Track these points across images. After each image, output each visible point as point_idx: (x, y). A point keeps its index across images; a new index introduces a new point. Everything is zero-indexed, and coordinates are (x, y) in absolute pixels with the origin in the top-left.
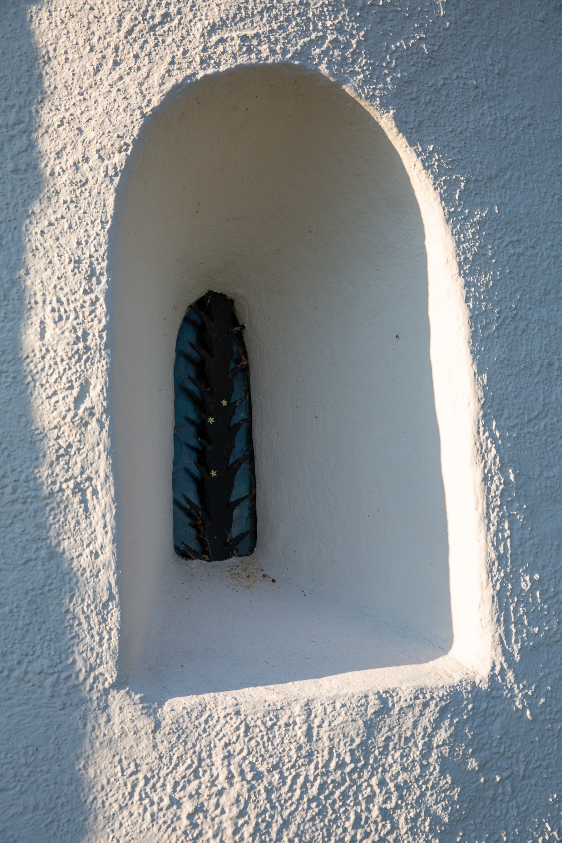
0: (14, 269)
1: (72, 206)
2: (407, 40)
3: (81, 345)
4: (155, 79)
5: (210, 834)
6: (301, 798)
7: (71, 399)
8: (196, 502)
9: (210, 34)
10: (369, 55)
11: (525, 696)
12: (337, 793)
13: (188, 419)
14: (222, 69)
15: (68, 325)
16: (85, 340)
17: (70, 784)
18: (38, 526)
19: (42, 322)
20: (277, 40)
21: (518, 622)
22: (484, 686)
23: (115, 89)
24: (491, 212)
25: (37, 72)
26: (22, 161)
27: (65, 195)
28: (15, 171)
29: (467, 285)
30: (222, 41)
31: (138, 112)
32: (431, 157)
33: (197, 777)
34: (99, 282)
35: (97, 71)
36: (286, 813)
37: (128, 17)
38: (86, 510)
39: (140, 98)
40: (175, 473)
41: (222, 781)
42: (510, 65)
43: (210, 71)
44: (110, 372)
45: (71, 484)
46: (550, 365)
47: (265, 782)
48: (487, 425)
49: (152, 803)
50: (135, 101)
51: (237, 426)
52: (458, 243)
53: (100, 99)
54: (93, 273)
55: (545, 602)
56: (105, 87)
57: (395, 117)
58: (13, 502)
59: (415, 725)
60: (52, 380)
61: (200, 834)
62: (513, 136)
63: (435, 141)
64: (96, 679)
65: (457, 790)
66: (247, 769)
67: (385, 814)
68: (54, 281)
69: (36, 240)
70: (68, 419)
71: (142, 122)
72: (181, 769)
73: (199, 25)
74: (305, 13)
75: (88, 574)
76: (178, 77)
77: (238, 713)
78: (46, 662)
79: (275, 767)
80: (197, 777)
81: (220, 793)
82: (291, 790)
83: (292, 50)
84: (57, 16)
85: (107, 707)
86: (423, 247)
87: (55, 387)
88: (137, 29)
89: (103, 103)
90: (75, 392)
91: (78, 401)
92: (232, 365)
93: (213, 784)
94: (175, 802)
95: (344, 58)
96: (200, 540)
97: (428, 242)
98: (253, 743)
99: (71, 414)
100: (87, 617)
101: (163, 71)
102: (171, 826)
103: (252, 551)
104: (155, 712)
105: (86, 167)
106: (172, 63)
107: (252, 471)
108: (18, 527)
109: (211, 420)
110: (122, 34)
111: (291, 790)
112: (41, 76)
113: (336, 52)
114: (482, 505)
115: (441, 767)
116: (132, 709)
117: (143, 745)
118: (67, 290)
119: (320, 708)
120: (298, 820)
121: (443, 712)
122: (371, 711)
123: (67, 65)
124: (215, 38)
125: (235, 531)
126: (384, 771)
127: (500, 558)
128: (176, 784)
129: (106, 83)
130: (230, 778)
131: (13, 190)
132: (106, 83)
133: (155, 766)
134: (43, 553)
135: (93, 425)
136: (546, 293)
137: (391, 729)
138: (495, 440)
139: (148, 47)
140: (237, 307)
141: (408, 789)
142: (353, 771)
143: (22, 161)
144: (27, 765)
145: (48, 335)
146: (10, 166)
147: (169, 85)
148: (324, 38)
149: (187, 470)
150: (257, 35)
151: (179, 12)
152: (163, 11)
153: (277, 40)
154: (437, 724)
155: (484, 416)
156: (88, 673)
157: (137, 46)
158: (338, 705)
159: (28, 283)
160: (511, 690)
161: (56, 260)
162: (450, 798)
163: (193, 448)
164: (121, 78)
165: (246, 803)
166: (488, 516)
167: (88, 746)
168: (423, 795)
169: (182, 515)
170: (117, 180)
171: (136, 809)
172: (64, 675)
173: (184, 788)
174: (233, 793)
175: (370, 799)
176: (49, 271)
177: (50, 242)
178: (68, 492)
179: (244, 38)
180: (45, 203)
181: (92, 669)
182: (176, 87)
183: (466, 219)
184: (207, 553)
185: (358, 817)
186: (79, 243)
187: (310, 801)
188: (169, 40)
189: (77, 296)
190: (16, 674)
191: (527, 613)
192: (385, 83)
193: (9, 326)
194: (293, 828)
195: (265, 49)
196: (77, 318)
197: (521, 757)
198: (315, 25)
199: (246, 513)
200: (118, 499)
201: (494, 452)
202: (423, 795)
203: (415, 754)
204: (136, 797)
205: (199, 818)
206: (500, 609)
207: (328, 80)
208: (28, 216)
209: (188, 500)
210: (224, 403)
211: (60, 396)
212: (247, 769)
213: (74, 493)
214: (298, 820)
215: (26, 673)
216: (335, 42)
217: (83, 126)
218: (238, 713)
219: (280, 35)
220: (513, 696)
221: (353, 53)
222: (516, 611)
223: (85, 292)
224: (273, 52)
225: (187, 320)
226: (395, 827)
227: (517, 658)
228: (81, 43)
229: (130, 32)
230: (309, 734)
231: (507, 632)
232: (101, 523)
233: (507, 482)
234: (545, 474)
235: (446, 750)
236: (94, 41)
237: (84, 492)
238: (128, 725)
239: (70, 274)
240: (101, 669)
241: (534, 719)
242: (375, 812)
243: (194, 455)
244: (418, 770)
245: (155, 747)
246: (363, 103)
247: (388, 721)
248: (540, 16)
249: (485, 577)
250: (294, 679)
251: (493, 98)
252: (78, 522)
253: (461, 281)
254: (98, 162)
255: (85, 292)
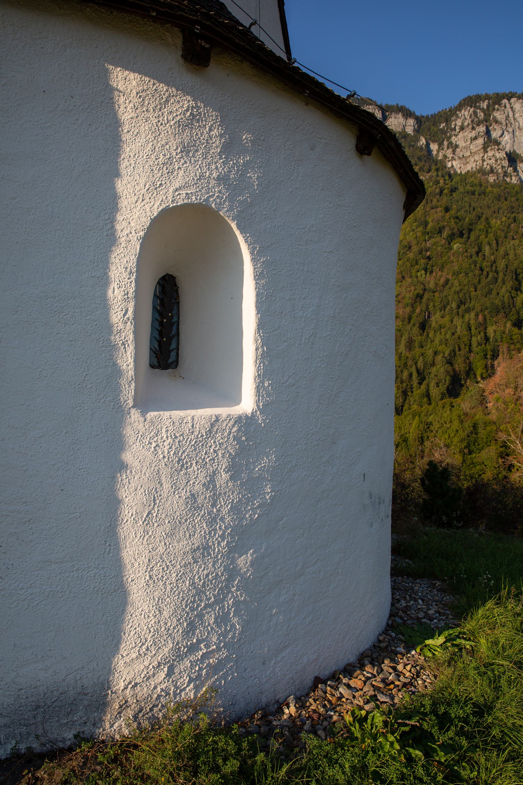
0: (105, 269)
1: (125, 249)
2: (243, 197)
3: (126, 297)
4: (156, 206)
5: (160, 453)
6: (189, 445)
7: (122, 314)
8: (157, 348)
9: (175, 192)
10: (229, 202)
11: (262, 419)
12: (200, 444)
13: (157, 319)
14: (179, 204)
15: (122, 289)
16: (128, 295)
17: (118, 435)
18: (110, 355)
19: (114, 288)
20: (198, 195)
21: (263, 396)
22: (250, 415)
23: (142, 209)
24: (267, 259)
25: (116, 202)
26: (110, 232)
27: (123, 245)
28: (107, 236)
29: (256, 283)
30: (179, 194)
31: (149, 218)
32: (248, 238)
33: (157, 436)
34: (133, 275)
35: (136, 202)
36: (184, 449)
37: (148, 184)
38: (125, 351)
39: (150, 213)
40: (151, 338)
41: (165, 438)
42: (278, 207)
43: (174, 205)
44: (135, 306)
45: (121, 342)
46: (282, 312)
47: (178, 439)
48: (259, 332)
49: (143, 443)
50: (149, 214)
51: (174, 323)
52: (255, 269)
53: (137, 212)
54: (131, 272)
55: (272, 390)
56: (138, 208)
57: (237, 224)
58: (102, 347)
59: (226, 426)
60: (116, 307)
61: (157, 453)
62: (277, 232)
63: (250, 233)
64: (127, 404)
65: (238, 446)
66: (173, 435)
67: (215, 451)
68: (118, 274)
69: (113, 260)
70: (121, 321)
71: (150, 221)
72: (152, 433)
73: (172, 188)
74: (208, 186)
75: (125, 371)
76: (164, 206)
77: (171, 418)
78: (111, 398)
79: (182, 435)
80: (157, 436)
81: (164, 441)
82: (186, 442)
83: (203, 198)
84: (124, 182)
85: (130, 413)
86: (243, 268)
87: (117, 310)
88: (151, 189)
89: (138, 214)
90: (124, 312)
91: (125, 315)
92: (174, 301)
93: (162, 439)
94: (150, 443)
95: (221, 202)
96: (158, 362)
97: (245, 267)
98: (175, 427)
99: (122, 319)
100: (125, 385)
101: (159, 204)
102: (148, 450)
103: (176, 367)
104: (145, 416)
105: (131, 235)
106: (162, 201)
107: (178, 339)
108: (103, 355)
109: (165, 320)
110: (145, 190)
111: (186, 442)
112: (117, 203)
113: (218, 200)
114: (255, 358)
115: (234, 438)
116: (138, 414)
117: (141, 425)
118: (122, 277)
119: (197, 419)
120: (188, 451)
121: (236, 422)
122: (213, 420)
123: (126, 200)
124: (177, 193)
125: (170, 361)
126: (216, 439)
127: (259, 375)
128: (151, 438)
129: (139, 207)
130: (167, 437)
131: (106, 242)
132: (139, 207)
133: (144, 432)
134: (111, 364)
135: (129, 323)
136: (283, 288)
137: (219, 426)
138: (261, 337)
139: (154, 195)
140: (176, 280)
141: (223, 444)
142: (206, 438)
143: (110, 232)
144: (105, 428)
145: (115, 292)
146: (105, 234)
147: (160, 209)
148: (214, 195)
149: (155, 337)
150: (191, 193)
151: (165, 183)
152: (160, 183)
153: (198, 195)
154: (233, 426)
155: (258, 328)
156: (124, 402)
157: (150, 195)
158: (203, 418)
159: (110, 274)
160: (258, 417)
161: (119, 267)
162: (236, 448)
163: (158, 330)
164: (144, 205)
165: (172, 445)
166: (256, 361)
167: (124, 424)
168: (227, 446)
169: (152, 353)
170: (141, 241)
171: (138, 444)
172: (117, 402)
173: (153, 439)
174: (168, 442)
175: (210, 447)
176: (117, 271)
177: (118, 261)
178: (120, 345)
179: (187, 194)
180: (116, 247)
181: (126, 401)
182: (163, 210)
183: (258, 260)
184: (161, 367)
185: (206, 452)
186: (127, 262)
187: (192, 446)
188: (161, 193)
189: (126, 280)
190: (102, 401)
191: (266, 393)
192: (234, 212)
193: (103, 288)
194: (186, 453)
195: (194, 197)
196: (125, 287)
197: (259, 437)
198: (212, 190)
199: (175, 354)
200: (136, 348)
201: (260, 340)
202: (227, 446)
203: (226, 434)
204: (138, 441)
205: (157, 448)
206: (257, 392)
207: (214, 210)
208: (111, 251)
209: (155, 348)
210: (170, 314)
211: (119, 313)
212: (173, 435)
213: (122, 345)
214: (188, 451)
215: (105, 401)
216: (218, 196)
217: (130, 221)
218: (171, 418)
219: (199, 193)
220: (259, 419)
221: (224, 201)
222: (262, 392)
223: (128, 279)
224: (196, 199)
225: (158, 283)
226: (217, 455)
227: (261, 407)
228: (131, 192)
229: (148, 189)
230: (193, 426)
231: (259, 399)
232: (130, 356)
233: (263, 351)
234: (276, 349)
235: (235, 434)
236: (136, 192)
237: (125, 345)
238: (136, 419)
239: (123, 272)
240: (128, 401)
241: (264, 426)
242: (212, 450)
243: (158, 332)
244: (226, 439)
245: (144, 426)
246: (226, 218)
247: (218, 424)
248: (290, 190)
249: (253, 381)
250: (189, 409)
251: (271, 219)
252: (123, 355)
253: (254, 282)
254: (135, 234)
255: (128, 279)
